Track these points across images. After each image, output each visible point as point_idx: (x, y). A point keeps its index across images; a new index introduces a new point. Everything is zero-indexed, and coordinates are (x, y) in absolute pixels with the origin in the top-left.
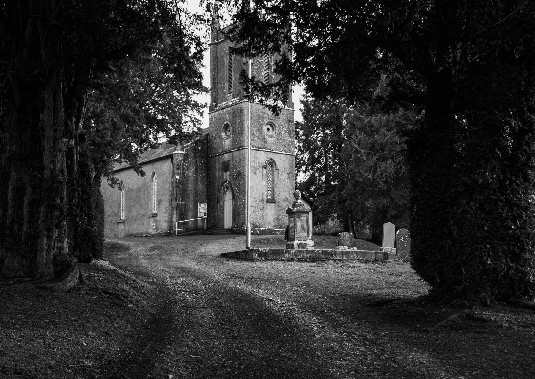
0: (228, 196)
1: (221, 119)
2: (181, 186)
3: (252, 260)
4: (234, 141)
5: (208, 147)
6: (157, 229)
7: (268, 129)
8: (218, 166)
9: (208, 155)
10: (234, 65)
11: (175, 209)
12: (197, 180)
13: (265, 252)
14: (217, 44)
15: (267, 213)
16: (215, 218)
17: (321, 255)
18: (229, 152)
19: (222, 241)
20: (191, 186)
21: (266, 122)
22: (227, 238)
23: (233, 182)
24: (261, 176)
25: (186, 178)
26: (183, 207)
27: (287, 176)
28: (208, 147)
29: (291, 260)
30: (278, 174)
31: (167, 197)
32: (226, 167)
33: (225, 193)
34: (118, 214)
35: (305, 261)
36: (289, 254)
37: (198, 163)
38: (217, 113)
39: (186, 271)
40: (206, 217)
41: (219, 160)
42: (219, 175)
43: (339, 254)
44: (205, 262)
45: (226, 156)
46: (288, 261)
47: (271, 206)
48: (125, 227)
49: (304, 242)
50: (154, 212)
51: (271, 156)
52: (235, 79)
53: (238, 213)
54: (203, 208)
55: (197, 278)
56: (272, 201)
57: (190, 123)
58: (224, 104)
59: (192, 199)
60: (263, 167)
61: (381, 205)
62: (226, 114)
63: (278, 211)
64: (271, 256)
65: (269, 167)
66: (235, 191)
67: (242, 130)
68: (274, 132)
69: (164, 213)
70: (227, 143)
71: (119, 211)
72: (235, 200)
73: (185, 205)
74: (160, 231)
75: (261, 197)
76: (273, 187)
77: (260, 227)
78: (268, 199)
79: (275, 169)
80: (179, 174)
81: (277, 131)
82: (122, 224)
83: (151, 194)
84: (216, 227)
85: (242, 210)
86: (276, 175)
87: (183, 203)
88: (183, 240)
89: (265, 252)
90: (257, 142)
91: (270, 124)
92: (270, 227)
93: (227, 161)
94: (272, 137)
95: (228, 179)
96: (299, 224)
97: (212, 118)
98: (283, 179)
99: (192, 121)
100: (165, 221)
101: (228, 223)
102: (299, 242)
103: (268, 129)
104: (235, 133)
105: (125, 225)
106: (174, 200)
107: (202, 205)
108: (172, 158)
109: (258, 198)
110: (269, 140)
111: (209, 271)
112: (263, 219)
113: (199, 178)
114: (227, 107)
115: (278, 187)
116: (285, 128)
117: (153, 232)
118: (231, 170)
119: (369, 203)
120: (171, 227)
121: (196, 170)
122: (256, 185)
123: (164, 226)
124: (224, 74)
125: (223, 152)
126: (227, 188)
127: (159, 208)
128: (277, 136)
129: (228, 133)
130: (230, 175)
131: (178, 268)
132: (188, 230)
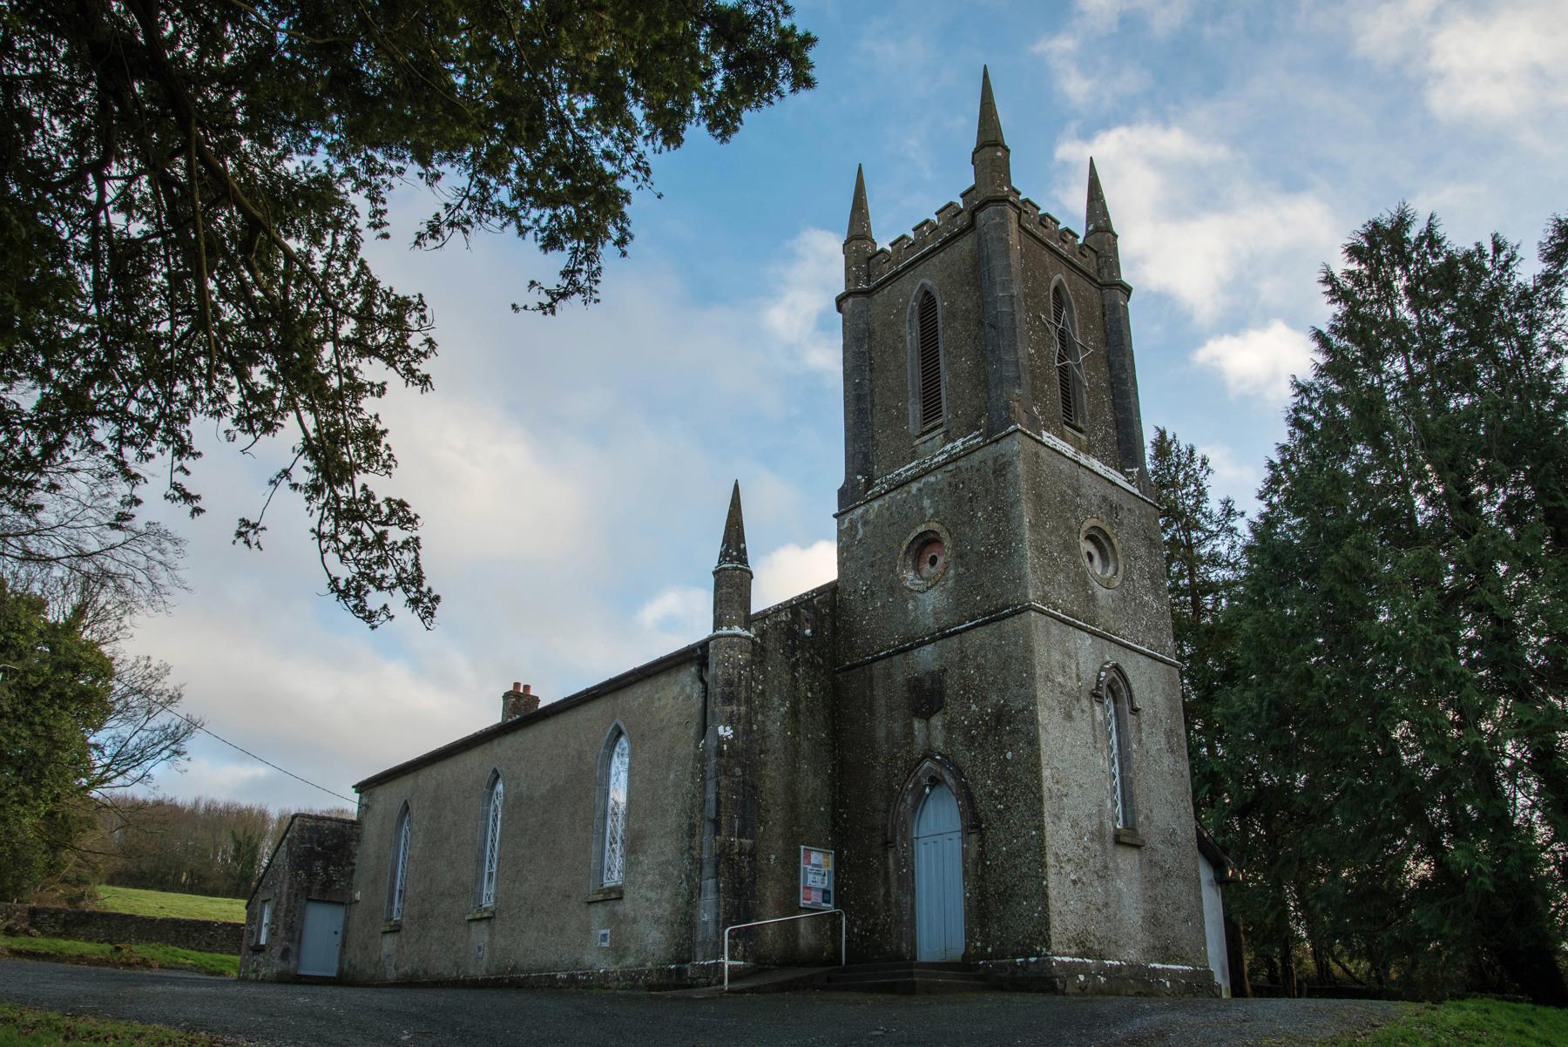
2: (738, 771)
6: (618, 950)
11: (708, 870)
14: (867, 293)
18: (942, 635)
20: (773, 777)
21: (1087, 525)
23: (965, 757)
24: (1089, 730)
26: (746, 859)
28: (835, 631)
30: (1139, 730)
31: (672, 820)
32: (926, 697)
33: (920, 799)
37: (802, 686)
38: (876, 504)
41: (889, 676)
42: (890, 733)
45: (927, 657)
47: (1128, 861)
51: (1112, 655)
52: (955, 376)
54: (817, 870)
56: (1128, 839)
59: (778, 830)
66: (978, 793)
68: (1111, 570)
69: (652, 886)
71: (478, 880)
72: (982, 833)
73: (752, 854)
74: (630, 961)
77: (1102, 957)
79: (1127, 708)
80: (730, 721)
82: (483, 925)
87: (747, 842)
92: (1132, 954)
93: (932, 674)
97: (853, 525)
100: (657, 921)
106: (709, 828)
107: (816, 857)
110: (1101, 592)
113: (805, 744)
118: (953, 707)
121: (794, 713)
123: (652, 941)
128: (1122, 584)
129: (926, 567)
130: (949, 728)
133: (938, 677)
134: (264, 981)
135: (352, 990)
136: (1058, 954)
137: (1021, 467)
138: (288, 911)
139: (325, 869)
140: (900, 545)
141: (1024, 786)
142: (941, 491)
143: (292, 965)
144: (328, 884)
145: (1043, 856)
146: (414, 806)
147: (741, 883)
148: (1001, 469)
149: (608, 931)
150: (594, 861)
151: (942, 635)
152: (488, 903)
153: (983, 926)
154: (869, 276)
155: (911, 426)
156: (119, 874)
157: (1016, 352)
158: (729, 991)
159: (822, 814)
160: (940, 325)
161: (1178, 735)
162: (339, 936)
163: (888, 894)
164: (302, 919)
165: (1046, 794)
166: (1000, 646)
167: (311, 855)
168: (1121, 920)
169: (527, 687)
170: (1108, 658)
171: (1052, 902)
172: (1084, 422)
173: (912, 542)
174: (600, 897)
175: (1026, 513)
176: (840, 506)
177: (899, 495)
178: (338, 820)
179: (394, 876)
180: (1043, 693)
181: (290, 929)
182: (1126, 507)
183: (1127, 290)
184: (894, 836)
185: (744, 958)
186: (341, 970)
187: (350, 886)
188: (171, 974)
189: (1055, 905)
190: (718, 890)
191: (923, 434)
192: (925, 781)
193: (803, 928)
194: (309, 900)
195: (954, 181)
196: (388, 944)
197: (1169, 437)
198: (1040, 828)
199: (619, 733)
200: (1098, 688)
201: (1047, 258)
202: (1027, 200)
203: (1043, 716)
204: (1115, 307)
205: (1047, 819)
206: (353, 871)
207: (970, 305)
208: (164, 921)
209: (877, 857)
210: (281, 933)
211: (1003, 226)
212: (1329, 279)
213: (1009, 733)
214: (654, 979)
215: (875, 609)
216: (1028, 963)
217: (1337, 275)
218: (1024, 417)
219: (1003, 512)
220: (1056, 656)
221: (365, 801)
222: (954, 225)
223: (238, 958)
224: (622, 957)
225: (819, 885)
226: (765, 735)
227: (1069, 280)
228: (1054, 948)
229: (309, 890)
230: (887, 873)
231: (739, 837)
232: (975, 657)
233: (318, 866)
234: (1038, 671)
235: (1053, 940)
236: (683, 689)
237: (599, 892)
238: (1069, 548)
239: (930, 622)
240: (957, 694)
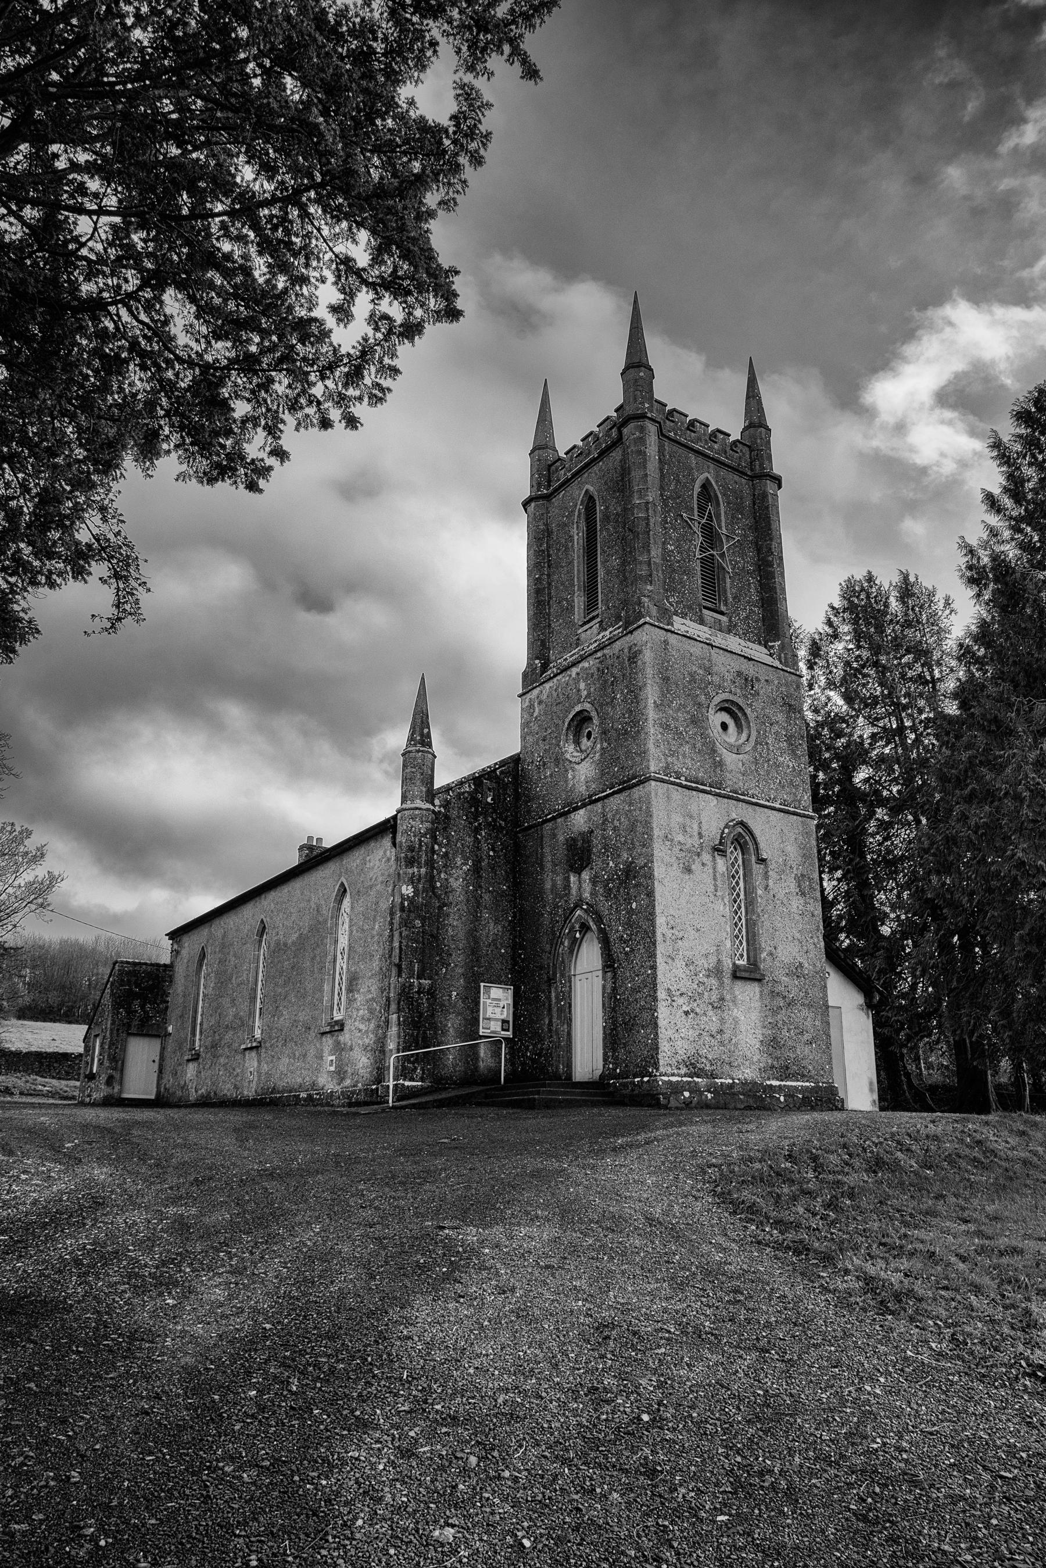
0: (587, 963)
1: (566, 699)
2: (418, 923)
5: (517, 797)
6: (340, 1074)
7: (724, 726)
8: (552, 852)
9: (516, 823)
11: (393, 1007)
12: (479, 905)
14: (547, 497)
15: (736, 1021)
16: (541, 1040)
18: (590, 801)
20: (455, 925)
21: (717, 699)
23: (604, 906)
24: (709, 880)
25: (438, 897)
28: (517, 797)
30: (766, 876)
31: (376, 964)
32: (579, 854)
33: (575, 944)
37: (485, 847)
38: (547, 686)
40: (509, 1034)
41: (554, 836)
42: (554, 885)
45: (580, 819)
47: (748, 994)
48: (259, 1062)
50: (338, 1017)
51: (739, 812)
52: (608, 572)
53: (628, 1021)
54: (496, 1005)
56: (749, 973)
58: (569, 657)
60: (715, 849)
62: (577, 681)
63: (775, 1012)
66: (613, 937)
68: (744, 736)
70: (583, 773)
71: (251, 1014)
73: (431, 993)
74: (348, 1082)
75: (713, 960)
76: (751, 925)
77: (713, 1076)
78: (736, 969)
79: (753, 858)
80: (411, 881)
81: (754, 734)
82: (254, 1054)
83: (330, 958)
85: (642, 1009)
86: (758, 881)
90: (688, 761)
91: (727, 707)
92: (748, 1073)
95: (587, 895)
97: (531, 706)
98: (781, 895)
101: (587, 1058)
103: (724, 726)
104: (613, 733)
105: (259, 1055)
108: (394, 833)
109: (702, 962)
110: (730, 759)
112: (722, 1043)
115: (767, 924)
116: (776, 728)
118: (597, 863)
121: (476, 870)
122: (689, 914)
124: (570, 572)
125: (569, 804)
126: (585, 928)
127: (350, 1001)
128: (755, 749)
129: (585, 743)
130: (594, 881)
132: (439, 1083)
133: (586, 837)
134: (94, 1105)
135: (176, 1110)
136: (665, 1075)
137: (647, 656)
138: (111, 1044)
139: (143, 1007)
140: (564, 722)
141: (642, 930)
142: (592, 675)
143: (116, 1090)
144: (145, 1021)
145: (655, 992)
146: (209, 950)
147: (420, 1017)
148: (634, 656)
149: (333, 1058)
150: (326, 998)
151: (590, 801)
153: (614, 1050)
154: (550, 479)
155: (576, 617)
156: (29, 1008)
157: (649, 551)
158: (393, 1107)
159: (502, 955)
160: (599, 528)
161: (810, 880)
162: (156, 1065)
163: (550, 1021)
164: (124, 1050)
165: (659, 938)
166: (630, 811)
167: (130, 995)
168: (736, 1045)
169: (319, 840)
170: (734, 816)
171: (662, 1031)
172: (726, 605)
173: (572, 720)
174: (328, 1029)
175: (651, 694)
176: (523, 688)
177: (562, 678)
178: (152, 965)
179: (196, 1011)
180: (661, 852)
181: (113, 1059)
182: (762, 678)
183: (778, 481)
184: (555, 974)
185: (422, 1080)
186: (158, 1093)
187: (165, 1021)
188: (30, 1100)
189: (665, 1032)
190: (399, 1024)
191: (585, 623)
192: (577, 926)
194: (129, 1034)
195: (609, 397)
196: (191, 1069)
197: (912, 579)
198: (654, 968)
200: (721, 843)
201: (693, 459)
202: (674, 410)
203: (659, 871)
204: (764, 495)
205: (660, 960)
206: (167, 1008)
207: (619, 509)
208: (29, 1054)
209: (543, 992)
210: (107, 1063)
211: (642, 440)
213: (636, 886)
214: (362, 1097)
215: (546, 777)
216: (642, 1082)
217: (1006, 439)
218: (654, 611)
219: (635, 694)
220: (677, 818)
221: (176, 947)
222: (609, 436)
223: (78, 1084)
224: (342, 1079)
225: (499, 1016)
226: (447, 890)
227: (717, 476)
228: (662, 1069)
229: (129, 1026)
230: (550, 1005)
231: (418, 978)
232: (612, 822)
233: (136, 1005)
234: (656, 832)
235: (661, 1062)
236: (385, 852)
237: (329, 1024)
238: (697, 722)
239: (582, 789)
240: (600, 852)
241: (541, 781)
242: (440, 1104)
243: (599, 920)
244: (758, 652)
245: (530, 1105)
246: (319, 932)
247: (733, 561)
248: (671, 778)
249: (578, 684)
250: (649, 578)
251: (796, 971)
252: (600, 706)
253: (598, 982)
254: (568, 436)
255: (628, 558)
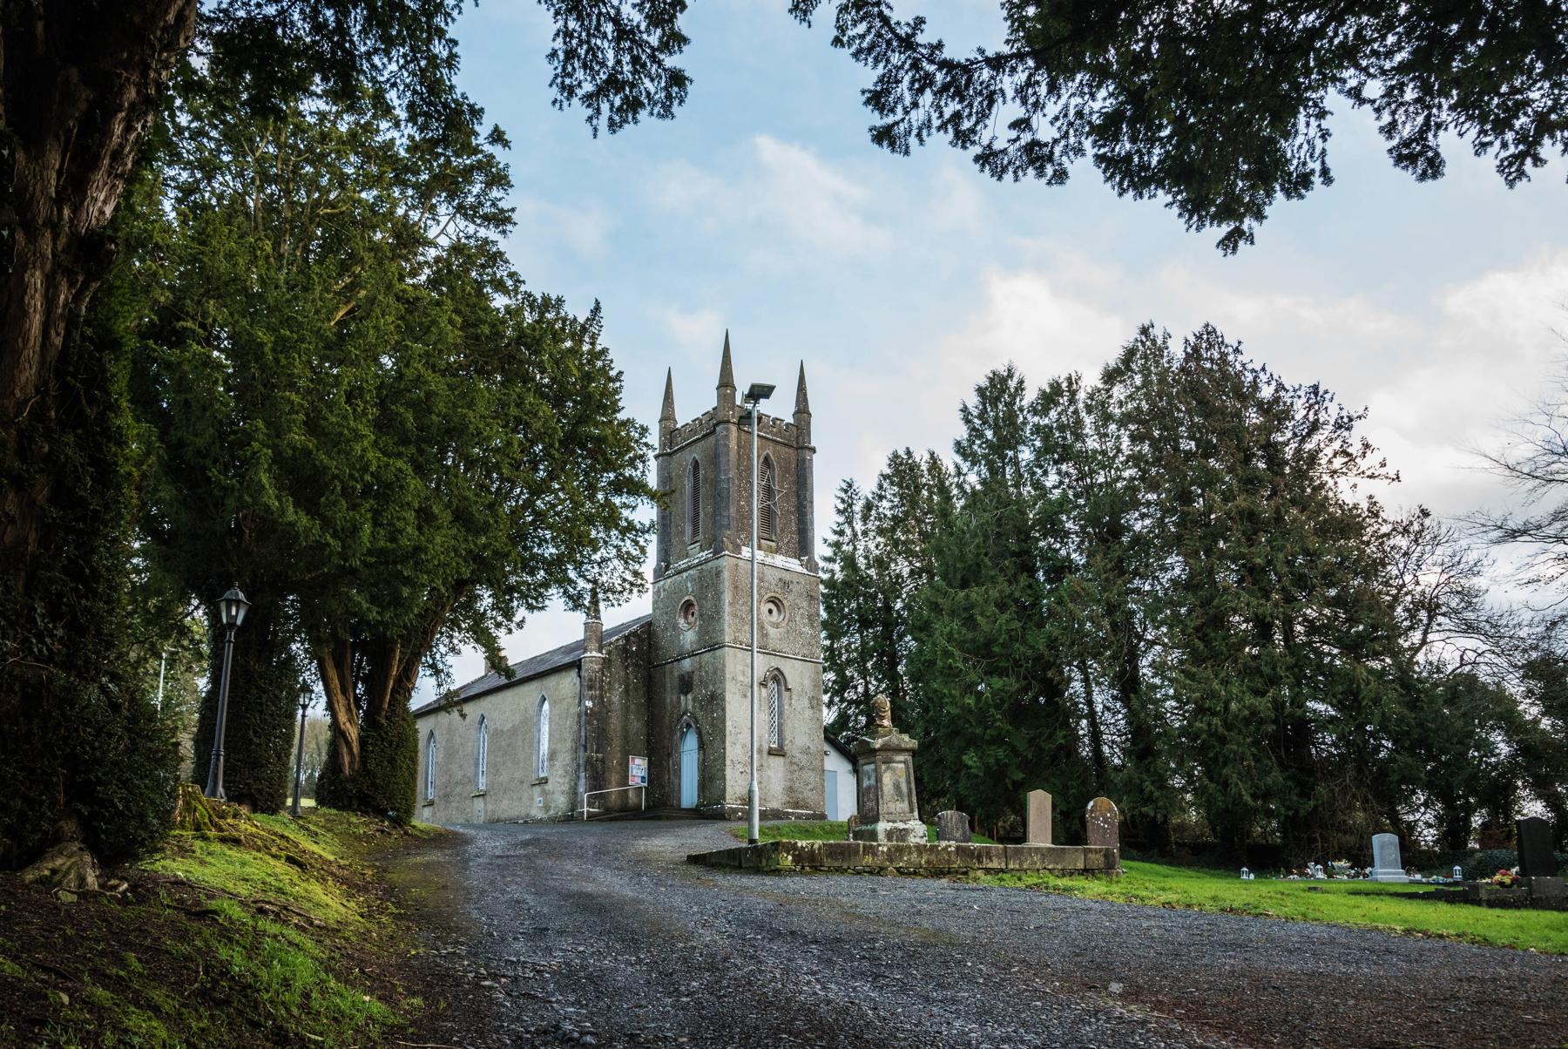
0: (690, 743)
1: (678, 591)
3: (777, 872)
4: (703, 632)
6: (547, 808)
7: (770, 611)
8: (671, 682)
10: (702, 491)
13: (812, 851)
17: (953, 858)
18: (692, 655)
19: (680, 832)
20: (615, 723)
22: (689, 826)
23: (700, 714)
27: (806, 703)
28: (650, 646)
29: (880, 871)
31: (569, 744)
32: (686, 685)
33: (683, 735)
34: (473, 781)
35: (915, 873)
36: (874, 854)
39: (592, 907)
43: (998, 856)
44: (651, 878)
45: (687, 664)
46: (871, 873)
47: (777, 762)
49: (901, 826)
50: (542, 775)
51: (776, 662)
53: (711, 776)
54: (638, 768)
55: (632, 942)
56: (778, 752)
57: (616, 562)
58: (683, 564)
61: (992, 760)
64: (827, 862)
65: (772, 685)
67: (718, 610)
70: (689, 638)
71: (476, 774)
73: (603, 761)
76: (780, 725)
80: (591, 698)
84: (665, 804)
86: (786, 701)
88: (598, 828)
89: (812, 851)
91: (773, 601)
94: (776, 625)
96: (887, 779)
99: (620, 556)
102: (889, 826)
103: (770, 611)
107: (638, 761)
108: (579, 668)
110: (772, 631)
111: (672, 909)
114: (689, 568)
117: (540, 815)
118: (696, 690)
119: (971, 759)
120: (574, 804)
121: (627, 691)
122: (744, 718)
123: (561, 802)
126: (689, 726)
127: (552, 766)
130: (694, 700)
131: (569, 896)
132: (608, 810)
137: (726, 574)
146: (436, 733)
148: (718, 573)
152: (482, 787)
175: (727, 597)
183: (813, 450)
193: (631, 794)
195: (709, 401)
199: (544, 699)
203: (728, 697)
204: (804, 460)
211: (727, 437)
212: (965, 410)
217: (969, 406)
219: (718, 595)
226: (610, 702)
241: (665, 639)
242: (611, 820)
243: (697, 722)
244: (794, 564)
245: (660, 818)
246: (528, 726)
247: (782, 505)
248: (738, 645)
249: (687, 584)
250: (728, 527)
251: (806, 751)
252: (699, 599)
253: (696, 756)
254: (685, 415)
255: (716, 513)
